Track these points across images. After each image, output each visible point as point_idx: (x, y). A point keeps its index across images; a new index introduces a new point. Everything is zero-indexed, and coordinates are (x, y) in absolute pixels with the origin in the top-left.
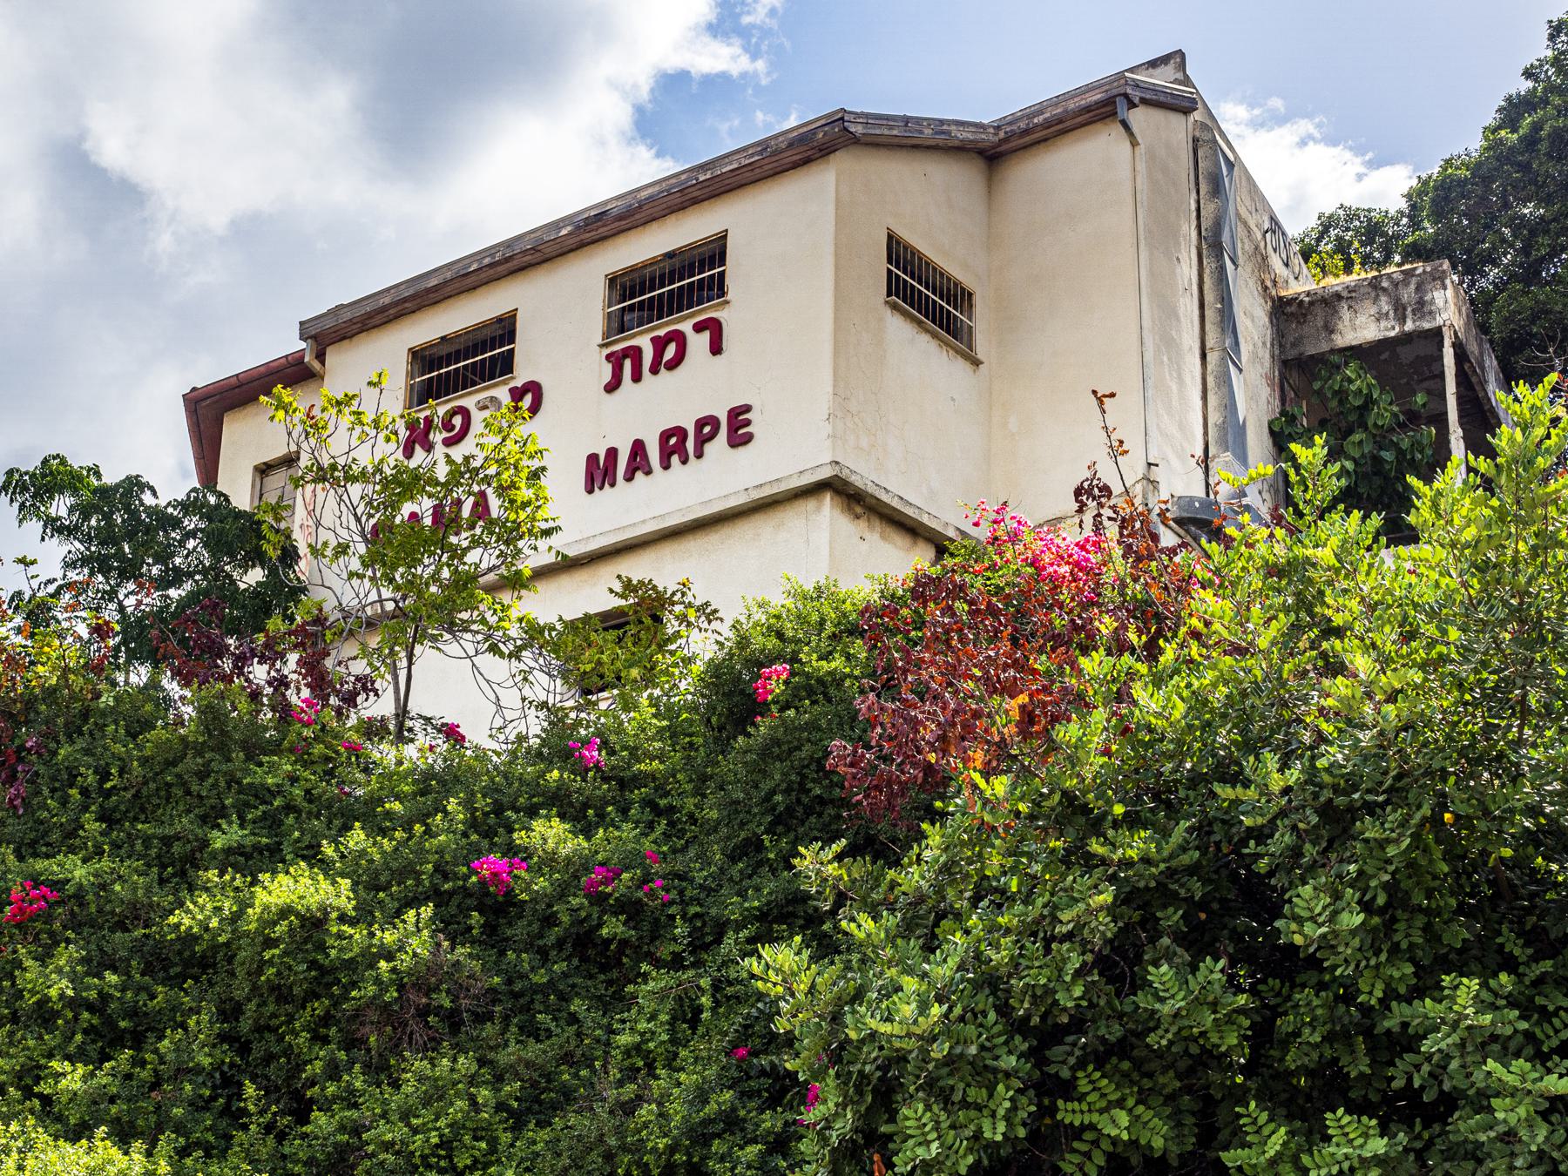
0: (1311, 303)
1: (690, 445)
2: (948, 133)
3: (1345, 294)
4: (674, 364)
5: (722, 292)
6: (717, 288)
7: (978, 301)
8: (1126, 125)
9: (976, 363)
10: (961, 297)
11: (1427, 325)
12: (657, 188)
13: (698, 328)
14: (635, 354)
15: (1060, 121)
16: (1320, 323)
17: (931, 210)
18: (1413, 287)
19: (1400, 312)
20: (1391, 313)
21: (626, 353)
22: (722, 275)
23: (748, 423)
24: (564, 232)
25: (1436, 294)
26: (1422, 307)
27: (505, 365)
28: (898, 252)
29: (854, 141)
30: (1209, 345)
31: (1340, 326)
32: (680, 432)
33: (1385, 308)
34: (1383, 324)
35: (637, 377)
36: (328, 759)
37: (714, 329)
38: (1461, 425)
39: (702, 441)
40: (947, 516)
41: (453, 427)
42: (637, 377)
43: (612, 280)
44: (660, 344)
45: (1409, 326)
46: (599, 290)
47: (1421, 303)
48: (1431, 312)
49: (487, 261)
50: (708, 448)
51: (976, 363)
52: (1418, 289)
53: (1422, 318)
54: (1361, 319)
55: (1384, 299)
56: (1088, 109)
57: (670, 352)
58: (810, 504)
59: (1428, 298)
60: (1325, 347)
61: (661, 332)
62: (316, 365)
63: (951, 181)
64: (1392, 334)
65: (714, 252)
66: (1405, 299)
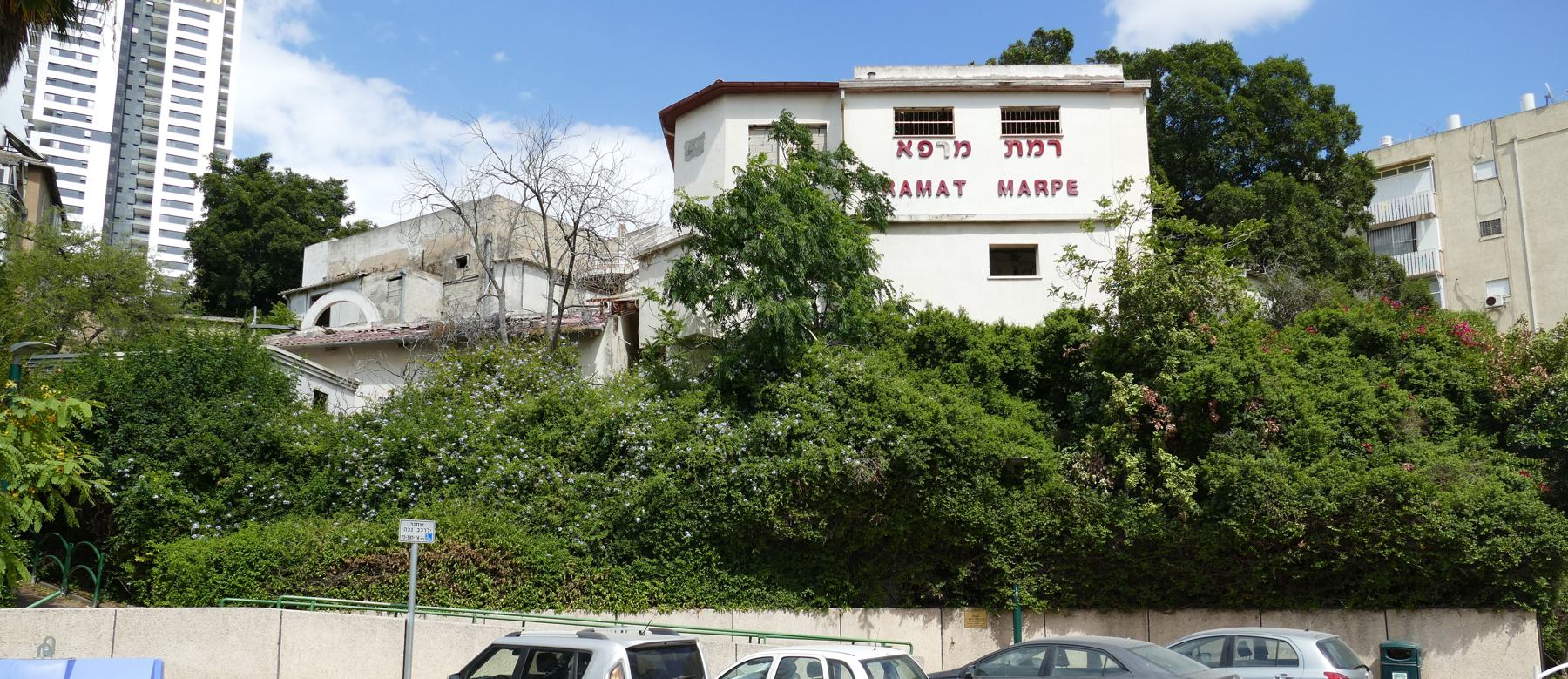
4: (965, 155)
6: (1056, 128)
13: (1050, 143)
27: (948, 130)
35: (1020, 155)
42: (1020, 155)
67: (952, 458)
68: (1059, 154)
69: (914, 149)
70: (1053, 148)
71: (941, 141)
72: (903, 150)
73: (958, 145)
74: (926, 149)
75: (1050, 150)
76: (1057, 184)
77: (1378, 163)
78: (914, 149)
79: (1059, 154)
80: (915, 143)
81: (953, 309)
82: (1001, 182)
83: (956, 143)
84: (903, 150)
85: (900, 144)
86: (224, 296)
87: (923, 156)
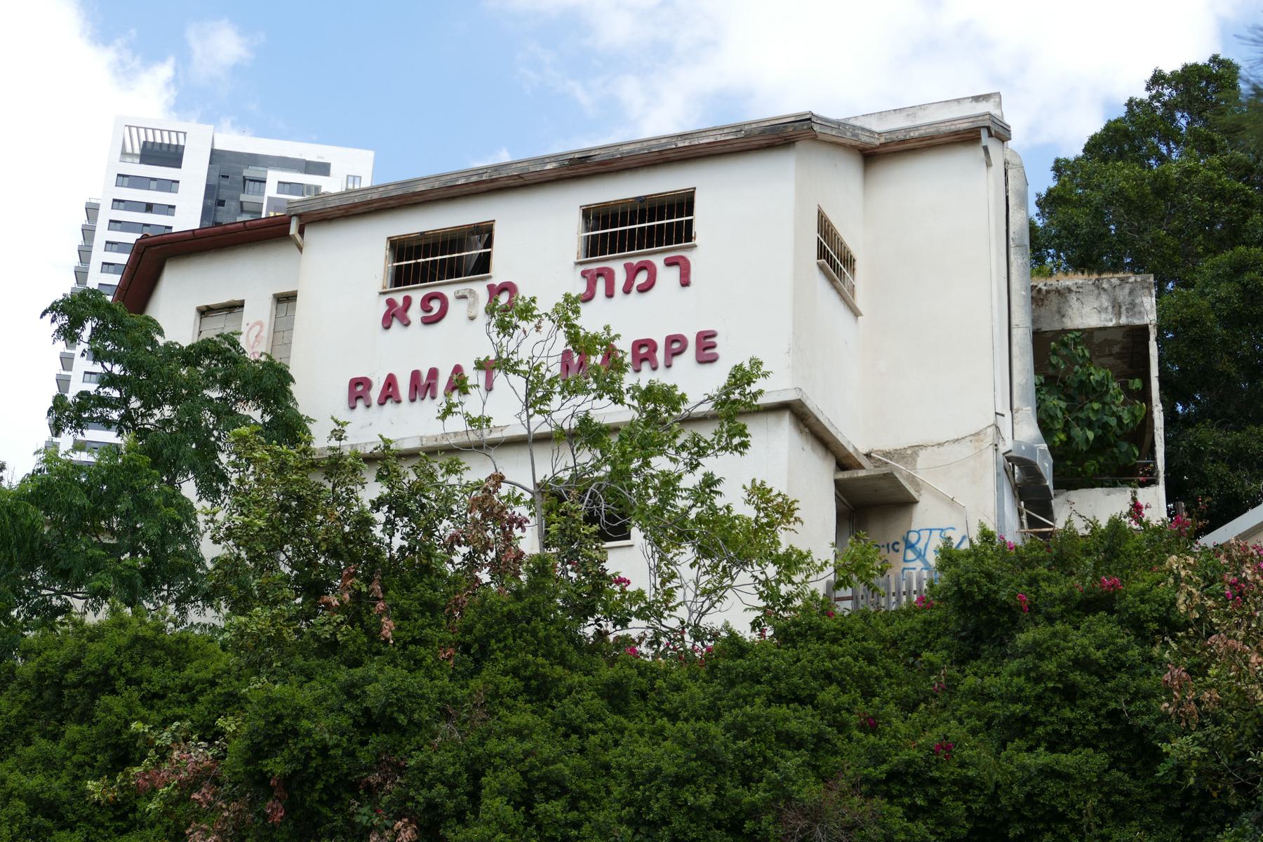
0: (1048, 292)
1: (660, 355)
2: (857, 135)
3: (1074, 288)
4: (644, 289)
5: (689, 237)
6: (685, 233)
7: (858, 265)
8: (986, 149)
9: (856, 313)
10: (849, 261)
11: (1137, 322)
12: (639, 146)
13: (670, 263)
14: (609, 276)
15: (932, 138)
16: (1055, 309)
17: (837, 188)
18: (1127, 291)
19: (1117, 307)
20: (1110, 309)
21: (600, 274)
22: (690, 223)
23: (713, 346)
24: (549, 167)
25: (1145, 299)
26: (1133, 307)
27: (483, 265)
28: (825, 228)
29: (814, 138)
30: (1014, 322)
31: (1070, 312)
32: (650, 344)
33: (1106, 304)
34: (1103, 316)
35: (610, 294)
36: (1207, 595)
37: (683, 266)
38: (1162, 401)
39: (672, 354)
40: (856, 439)
41: (430, 310)
42: (610, 294)
43: (587, 213)
44: (632, 272)
45: (1123, 321)
46: (577, 219)
47: (1133, 305)
48: (1140, 313)
49: (474, 179)
50: (677, 361)
51: (856, 313)
52: (1131, 293)
53: (1134, 315)
54: (1087, 309)
55: (1104, 298)
56: (956, 133)
57: (642, 278)
58: (771, 419)
59: (1138, 301)
60: (1057, 327)
61: (635, 261)
62: (298, 237)
63: (847, 172)
64: (1110, 324)
65: (684, 203)
66: (1121, 299)
67: (1237, 442)
68: (685, 283)
69: (415, 313)
70: (675, 272)
71: (462, 288)
72: (394, 315)
73: (495, 291)
74: (436, 305)
75: (668, 277)
76: (676, 344)
77: (507, 479)
78: (415, 313)
79: (685, 283)
80: (417, 296)
81: (1086, 141)
82: (713, 335)
83: (490, 287)
84: (394, 315)
85: (391, 303)
86: (464, 550)
87: (428, 322)
